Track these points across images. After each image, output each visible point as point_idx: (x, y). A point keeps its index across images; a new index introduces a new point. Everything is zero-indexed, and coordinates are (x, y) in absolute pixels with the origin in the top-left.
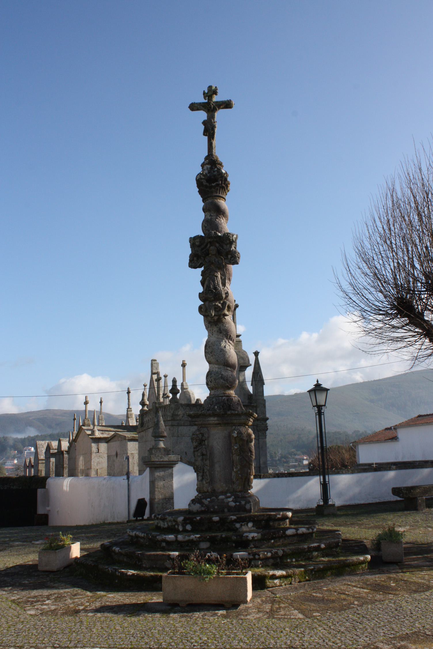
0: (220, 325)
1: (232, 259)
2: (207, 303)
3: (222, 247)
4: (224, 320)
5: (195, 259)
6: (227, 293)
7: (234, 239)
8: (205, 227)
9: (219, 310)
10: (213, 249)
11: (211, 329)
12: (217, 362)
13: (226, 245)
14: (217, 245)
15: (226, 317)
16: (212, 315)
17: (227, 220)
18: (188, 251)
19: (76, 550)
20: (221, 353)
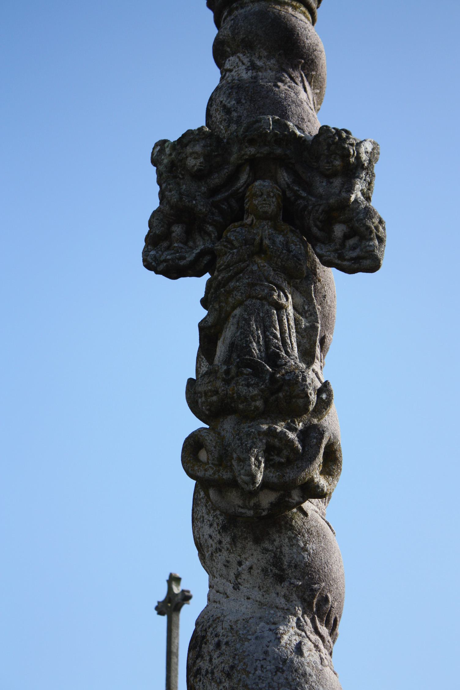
0: (281, 540)
1: (351, 242)
2: (228, 425)
3: (308, 186)
4: (298, 521)
7: (364, 157)
8: (228, 111)
9: (289, 462)
10: (264, 193)
11: (233, 558)
13: (329, 176)
14: (284, 177)
16: (253, 477)
17: (319, 97)
18: (146, 196)
19: (286, 133)
20: (281, 678)
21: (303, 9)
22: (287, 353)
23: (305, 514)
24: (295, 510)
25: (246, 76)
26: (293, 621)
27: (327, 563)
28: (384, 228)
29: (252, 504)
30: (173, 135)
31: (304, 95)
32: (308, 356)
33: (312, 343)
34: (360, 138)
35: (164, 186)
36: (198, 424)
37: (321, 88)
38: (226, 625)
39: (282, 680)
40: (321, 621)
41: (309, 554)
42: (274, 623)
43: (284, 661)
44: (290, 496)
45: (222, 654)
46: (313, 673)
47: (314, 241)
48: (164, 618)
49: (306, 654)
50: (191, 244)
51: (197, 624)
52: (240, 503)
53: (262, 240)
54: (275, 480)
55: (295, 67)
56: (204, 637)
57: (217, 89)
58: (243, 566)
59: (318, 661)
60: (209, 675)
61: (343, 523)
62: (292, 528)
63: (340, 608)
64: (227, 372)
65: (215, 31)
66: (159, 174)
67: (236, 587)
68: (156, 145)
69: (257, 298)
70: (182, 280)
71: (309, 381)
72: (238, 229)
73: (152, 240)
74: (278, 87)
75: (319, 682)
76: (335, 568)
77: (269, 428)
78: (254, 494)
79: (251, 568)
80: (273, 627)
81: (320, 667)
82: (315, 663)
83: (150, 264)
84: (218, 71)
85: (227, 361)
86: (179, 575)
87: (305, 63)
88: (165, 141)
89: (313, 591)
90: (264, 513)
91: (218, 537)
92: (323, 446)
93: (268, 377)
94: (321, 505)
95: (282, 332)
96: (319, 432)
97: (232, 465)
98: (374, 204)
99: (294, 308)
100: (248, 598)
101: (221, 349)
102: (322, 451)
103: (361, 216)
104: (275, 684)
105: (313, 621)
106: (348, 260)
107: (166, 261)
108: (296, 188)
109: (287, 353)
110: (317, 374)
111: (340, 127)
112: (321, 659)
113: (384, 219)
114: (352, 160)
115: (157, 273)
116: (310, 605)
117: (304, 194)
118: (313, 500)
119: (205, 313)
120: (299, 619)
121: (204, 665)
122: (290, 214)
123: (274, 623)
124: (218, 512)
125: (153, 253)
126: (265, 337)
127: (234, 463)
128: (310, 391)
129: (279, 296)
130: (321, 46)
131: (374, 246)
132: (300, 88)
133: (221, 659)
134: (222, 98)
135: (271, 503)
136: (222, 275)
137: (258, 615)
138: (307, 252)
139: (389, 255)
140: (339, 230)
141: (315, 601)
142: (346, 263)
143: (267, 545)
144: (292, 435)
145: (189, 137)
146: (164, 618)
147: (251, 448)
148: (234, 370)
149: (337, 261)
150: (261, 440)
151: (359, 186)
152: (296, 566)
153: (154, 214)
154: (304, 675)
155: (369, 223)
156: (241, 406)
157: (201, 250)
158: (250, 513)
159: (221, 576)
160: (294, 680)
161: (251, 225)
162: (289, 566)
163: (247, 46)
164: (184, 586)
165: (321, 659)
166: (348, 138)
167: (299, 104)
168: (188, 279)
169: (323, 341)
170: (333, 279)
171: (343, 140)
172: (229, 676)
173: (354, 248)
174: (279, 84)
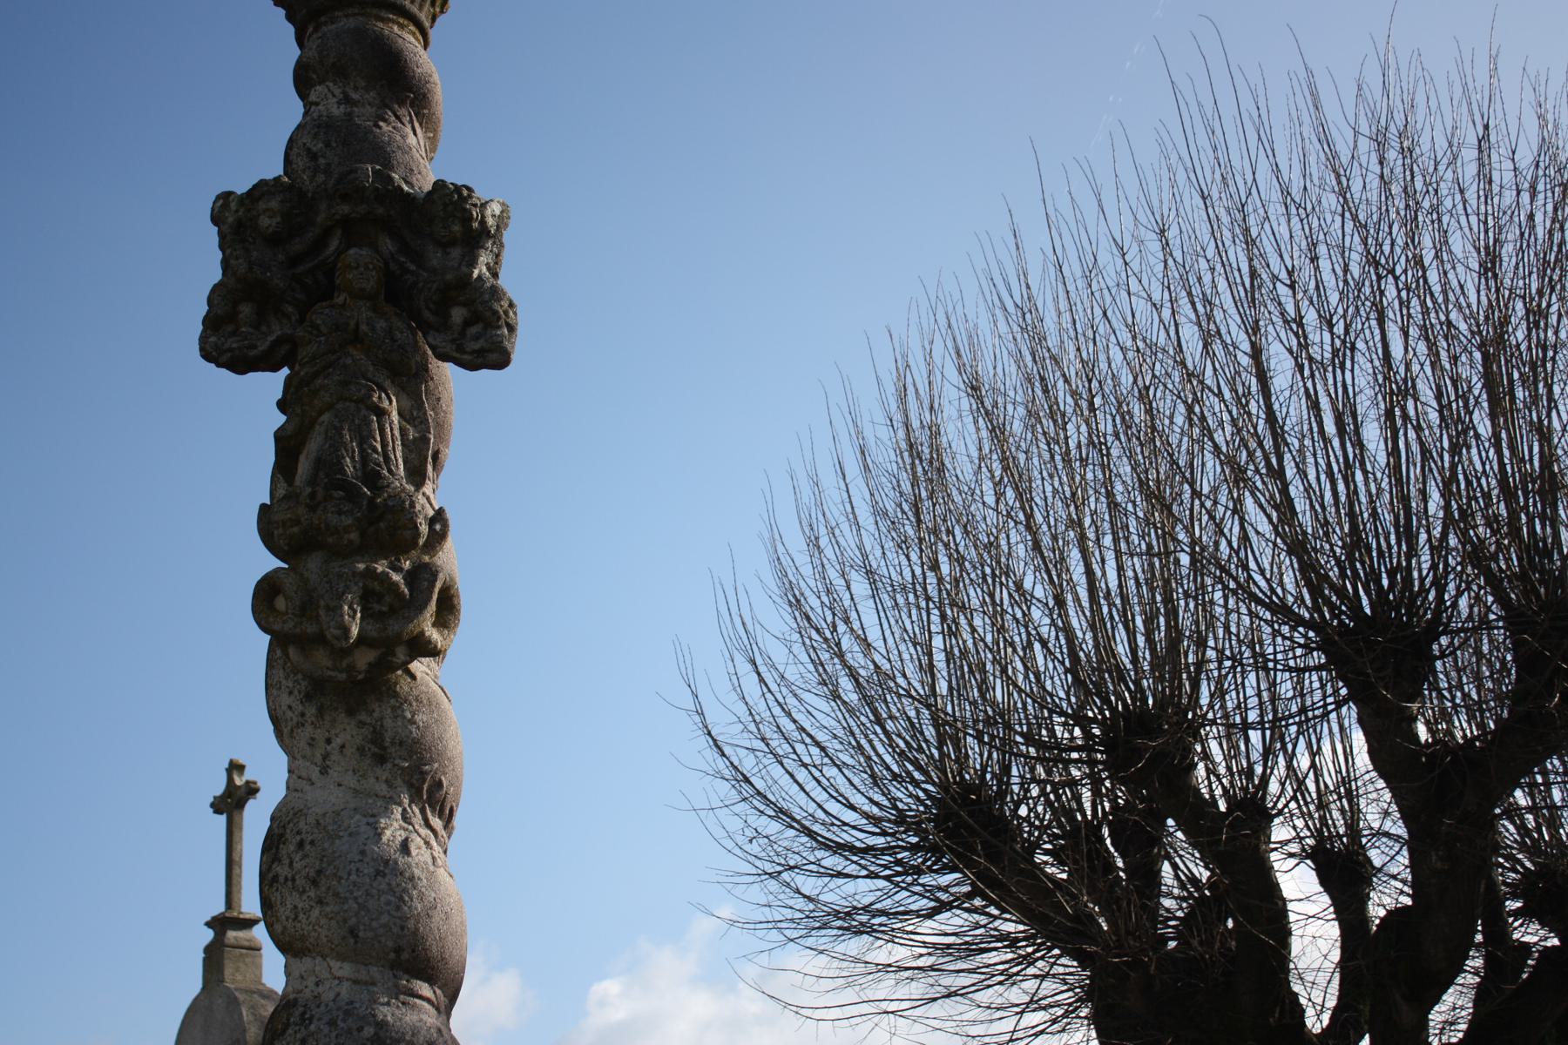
1: (474, 330)
2: (313, 564)
4: (404, 685)
6: (440, 515)
7: (490, 221)
9: (393, 611)
10: (361, 265)
11: (320, 735)
12: (353, 945)
14: (387, 245)
15: (418, 666)
16: (347, 631)
18: (202, 264)
21: (412, 28)
61: (462, 689)
139: (522, 347)
163: (340, 72)
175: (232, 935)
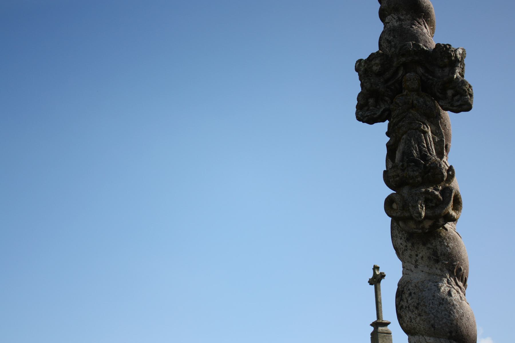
1: (456, 98)
2: (405, 191)
4: (443, 233)
5: (371, 101)
7: (459, 56)
8: (389, 42)
10: (411, 79)
11: (413, 253)
14: (420, 70)
16: (420, 214)
17: (433, 30)
18: (354, 86)
22: (430, 154)
23: (446, 230)
24: (441, 228)
25: (396, 24)
26: (445, 280)
27: (459, 252)
28: (472, 90)
29: (420, 227)
30: (365, 56)
31: (426, 30)
32: (441, 155)
33: (442, 148)
34: (456, 48)
35: (363, 81)
36: (390, 192)
37: (433, 26)
38: (413, 285)
39: (443, 308)
40: (459, 280)
41: (450, 248)
42: (436, 282)
43: (443, 299)
44: (439, 222)
45: (412, 298)
46: (457, 304)
47: (438, 99)
48: (373, 286)
49: (453, 295)
50: (378, 107)
51: (399, 285)
52: (415, 227)
53: (413, 101)
54: (431, 215)
55: (420, 17)
56: (403, 291)
57: (383, 32)
58: (419, 257)
59: (459, 298)
60: (407, 308)
61: (464, 232)
62: (441, 237)
63: (467, 273)
64: (403, 166)
65: (379, 5)
66: (360, 76)
67: (416, 267)
68: (357, 62)
69: (413, 129)
70: (376, 125)
71: (443, 166)
72: (400, 98)
73: (360, 107)
74: (413, 28)
75: (461, 308)
76: (463, 254)
77: (426, 190)
78: (421, 222)
79: (422, 257)
80: (436, 284)
81: (460, 301)
82: (458, 299)
83: (360, 118)
84: (382, 24)
85: (402, 160)
86: (378, 266)
87: (425, 15)
88: (361, 60)
89: (454, 266)
90: (427, 231)
91: (405, 244)
92: (453, 196)
93: (422, 166)
94: (453, 225)
95: (427, 144)
96: (450, 190)
97: (409, 209)
98: (466, 78)
99: (432, 132)
100: (422, 271)
101: (398, 155)
102: (452, 199)
103: (460, 85)
104: (440, 311)
105: (455, 280)
106: (456, 107)
107: (367, 116)
108: (427, 75)
109: (430, 154)
110: (445, 163)
111: (445, 44)
112: (461, 297)
113: (471, 85)
114: (453, 58)
115: (363, 122)
116: (453, 272)
117: (431, 77)
118: (449, 223)
119: (388, 139)
120: (448, 279)
121: (404, 304)
122: (424, 87)
123: (436, 282)
124: (404, 232)
125: (360, 113)
126: (419, 147)
127: (410, 208)
128: (444, 171)
129: (424, 127)
130: (432, 6)
131: (468, 98)
132: (423, 27)
133: (412, 301)
134: (386, 36)
135: (430, 226)
136: (395, 120)
137: (428, 279)
138: (435, 105)
139: (475, 102)
140: (450, 93)
141: (455, 270)
142: (454, 108)
143: (429, 245)
144: (437, 193)
145: (372, 57)
146: (373, 286)
147: (418, 200)
148: (405, 164)
149: (450, 108)
150: (422, 196)
151: (458, 70)
152: (444, 255)
153: (359, 95)
154: (453, 305)
155: (464, 88)
156: (411, 181)
157: (384, 110)
158: (420, 231)
159: (408, 262)
160: (448, 308)
161: (406, 95)
162: (441, 255)
163: (396, 10)
164: (381, 270)
165: (461, 297)
166: (450, 48)
167: (424, 34)
168: (378, 123)
169: (446, 146)
170: (449, 116)
171: (448, 49)
172: (417, 308)
173: (458, 101)
174: (413, 26)
175: (380, 329)
